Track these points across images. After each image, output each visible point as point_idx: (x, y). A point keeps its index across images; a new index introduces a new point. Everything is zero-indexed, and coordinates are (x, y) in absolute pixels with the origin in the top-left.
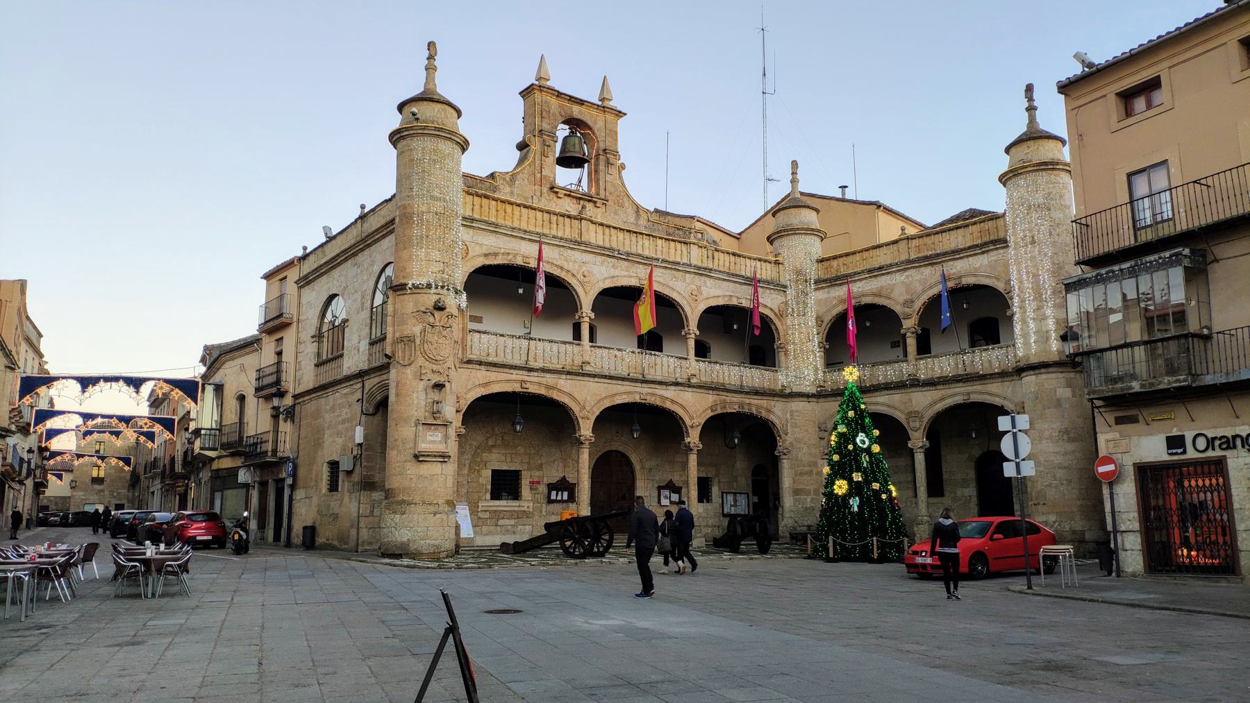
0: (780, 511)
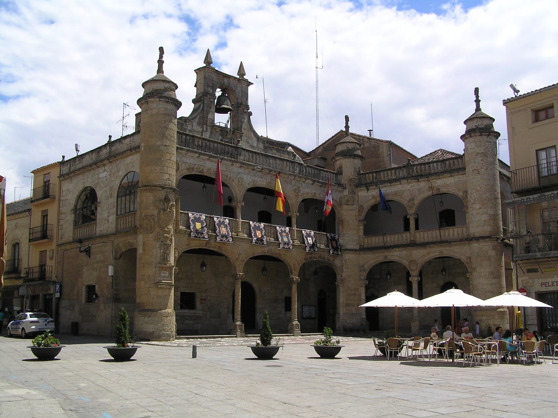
0: (337, 315)
